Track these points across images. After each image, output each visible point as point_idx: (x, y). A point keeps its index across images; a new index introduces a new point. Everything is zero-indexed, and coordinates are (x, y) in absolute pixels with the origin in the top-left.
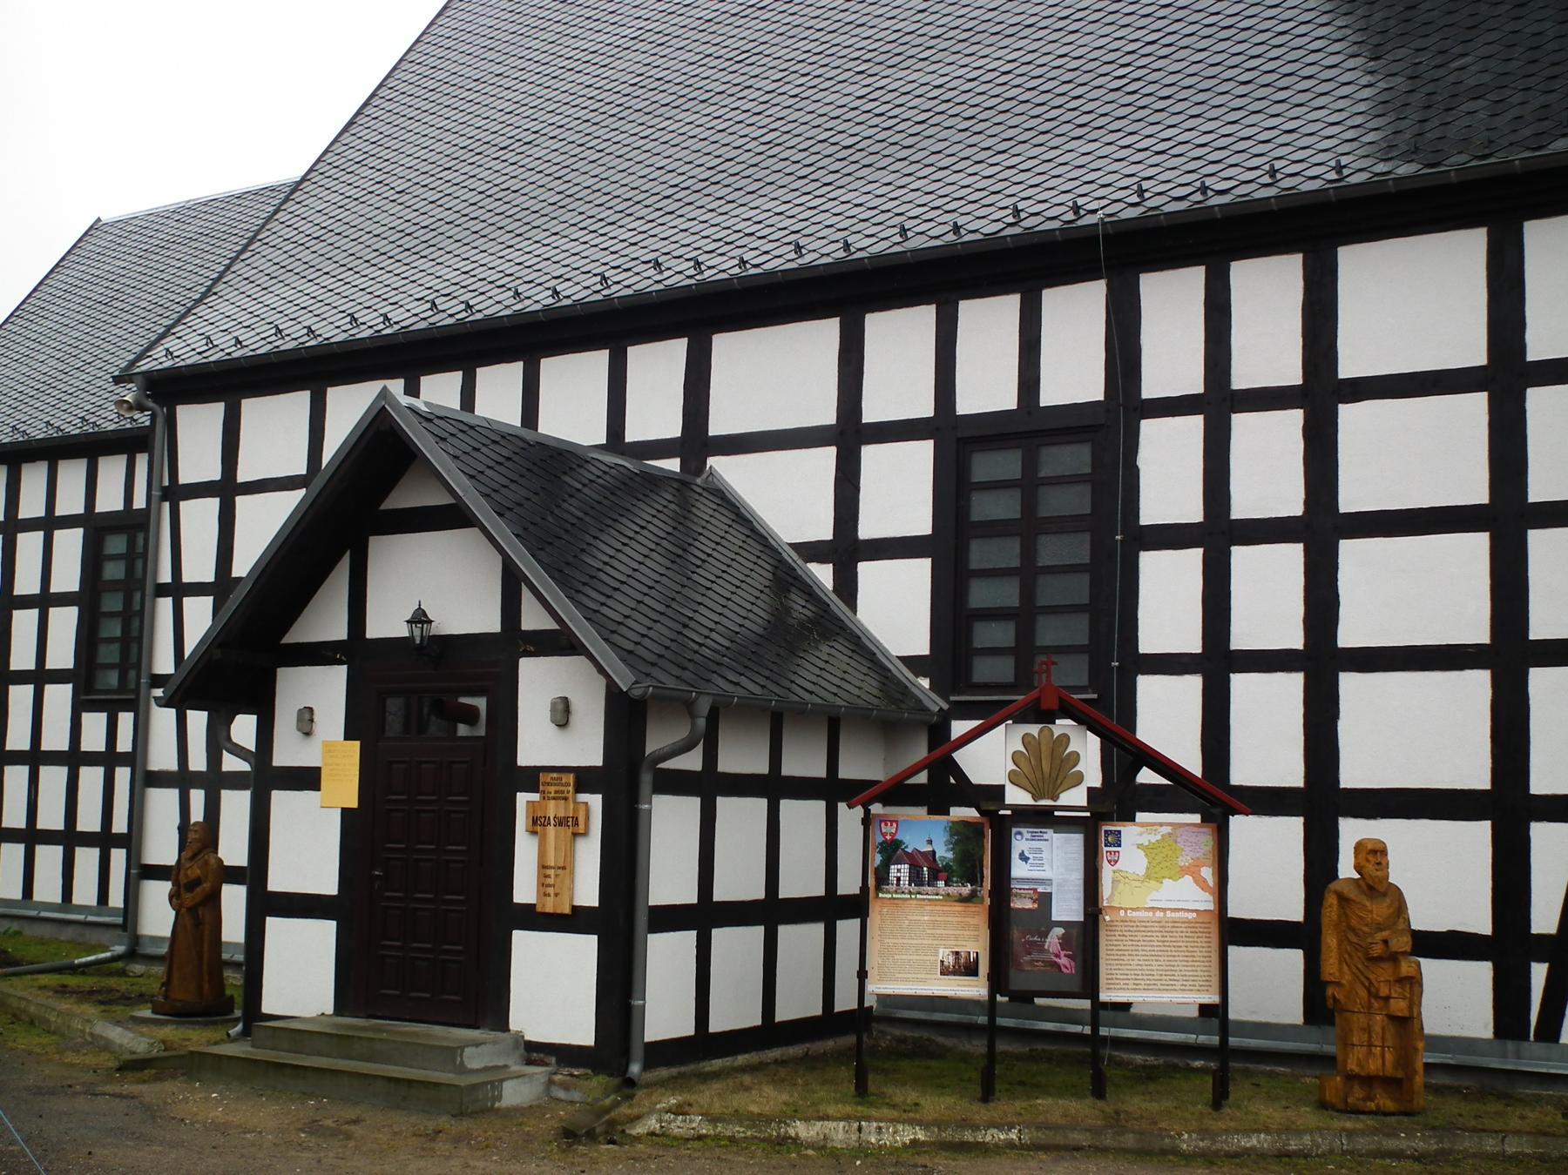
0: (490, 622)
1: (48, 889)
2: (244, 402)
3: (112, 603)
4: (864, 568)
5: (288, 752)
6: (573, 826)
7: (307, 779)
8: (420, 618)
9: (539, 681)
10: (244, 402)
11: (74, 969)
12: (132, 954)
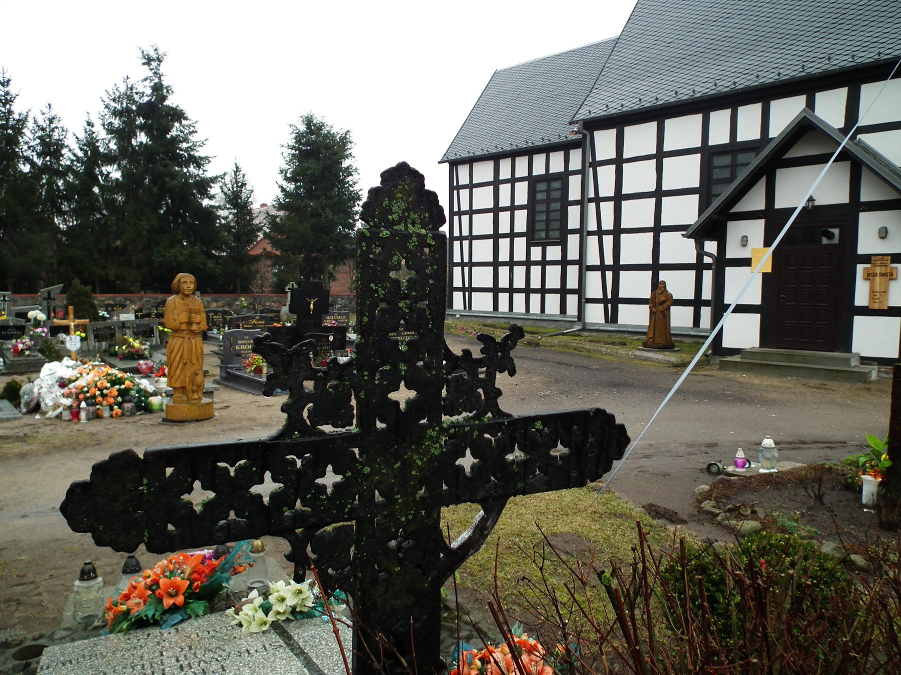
0: (843, 197)
1: (535, 308)
2: (626, 128)
3: (541, 208)
4: (664, 199)
5: (732, 252)
7: (745, 262)
8: (811, 199)
10: (626, 128)
11: (564, 334)
12: (584, 329)
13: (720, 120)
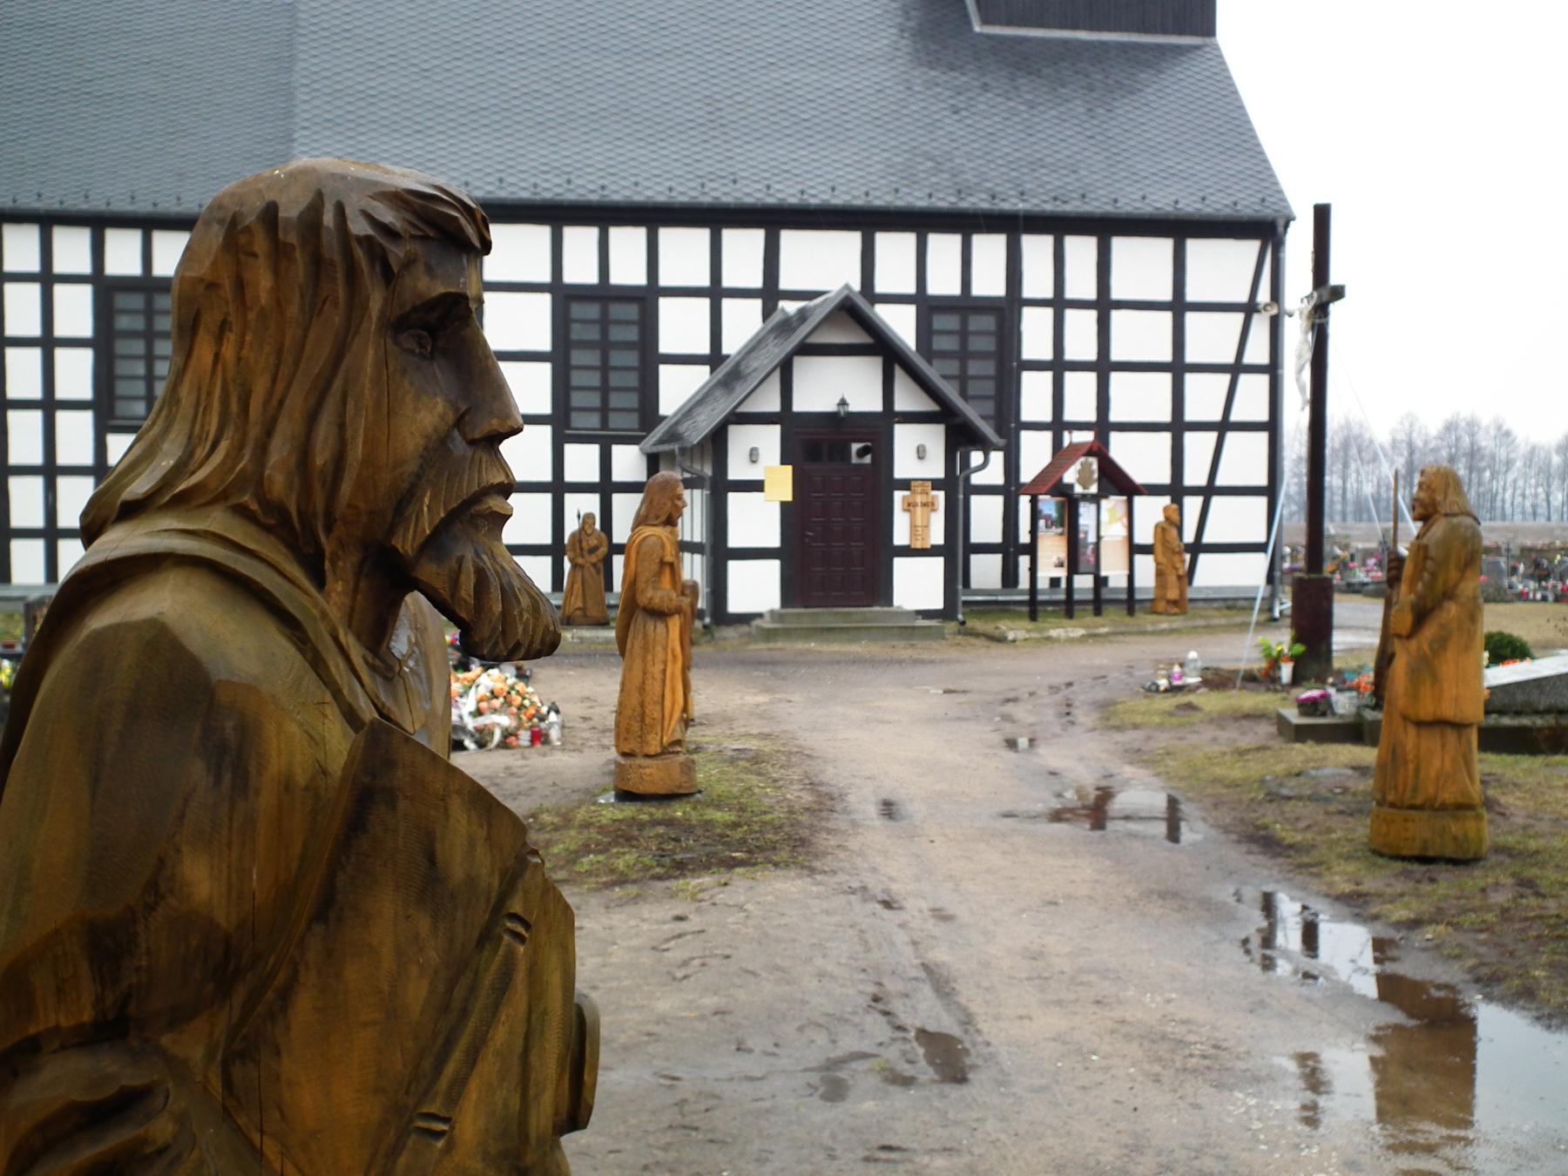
0: (876, 406)
6: (930, 506)
7: (756, 486)
8: (843, 403)
9: (906, 438)
13: (580, 241)
